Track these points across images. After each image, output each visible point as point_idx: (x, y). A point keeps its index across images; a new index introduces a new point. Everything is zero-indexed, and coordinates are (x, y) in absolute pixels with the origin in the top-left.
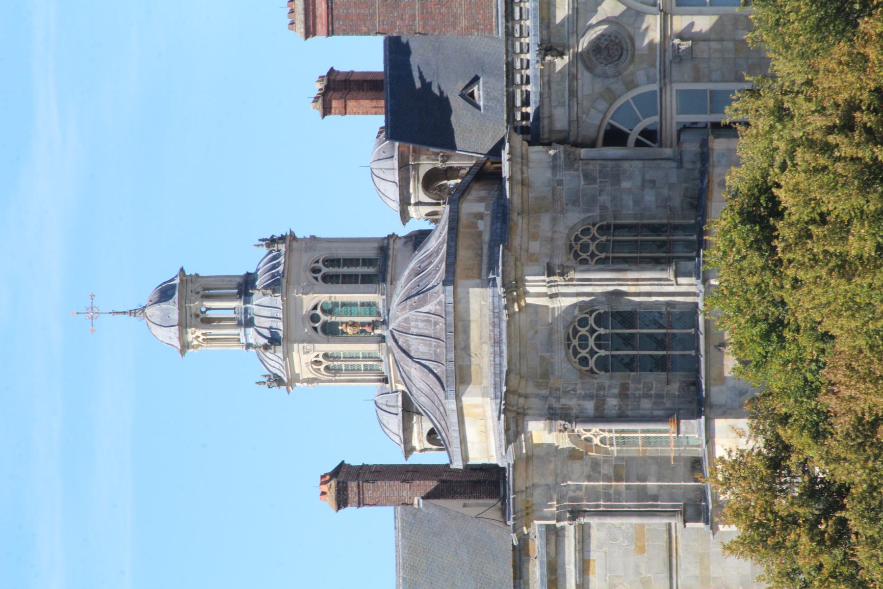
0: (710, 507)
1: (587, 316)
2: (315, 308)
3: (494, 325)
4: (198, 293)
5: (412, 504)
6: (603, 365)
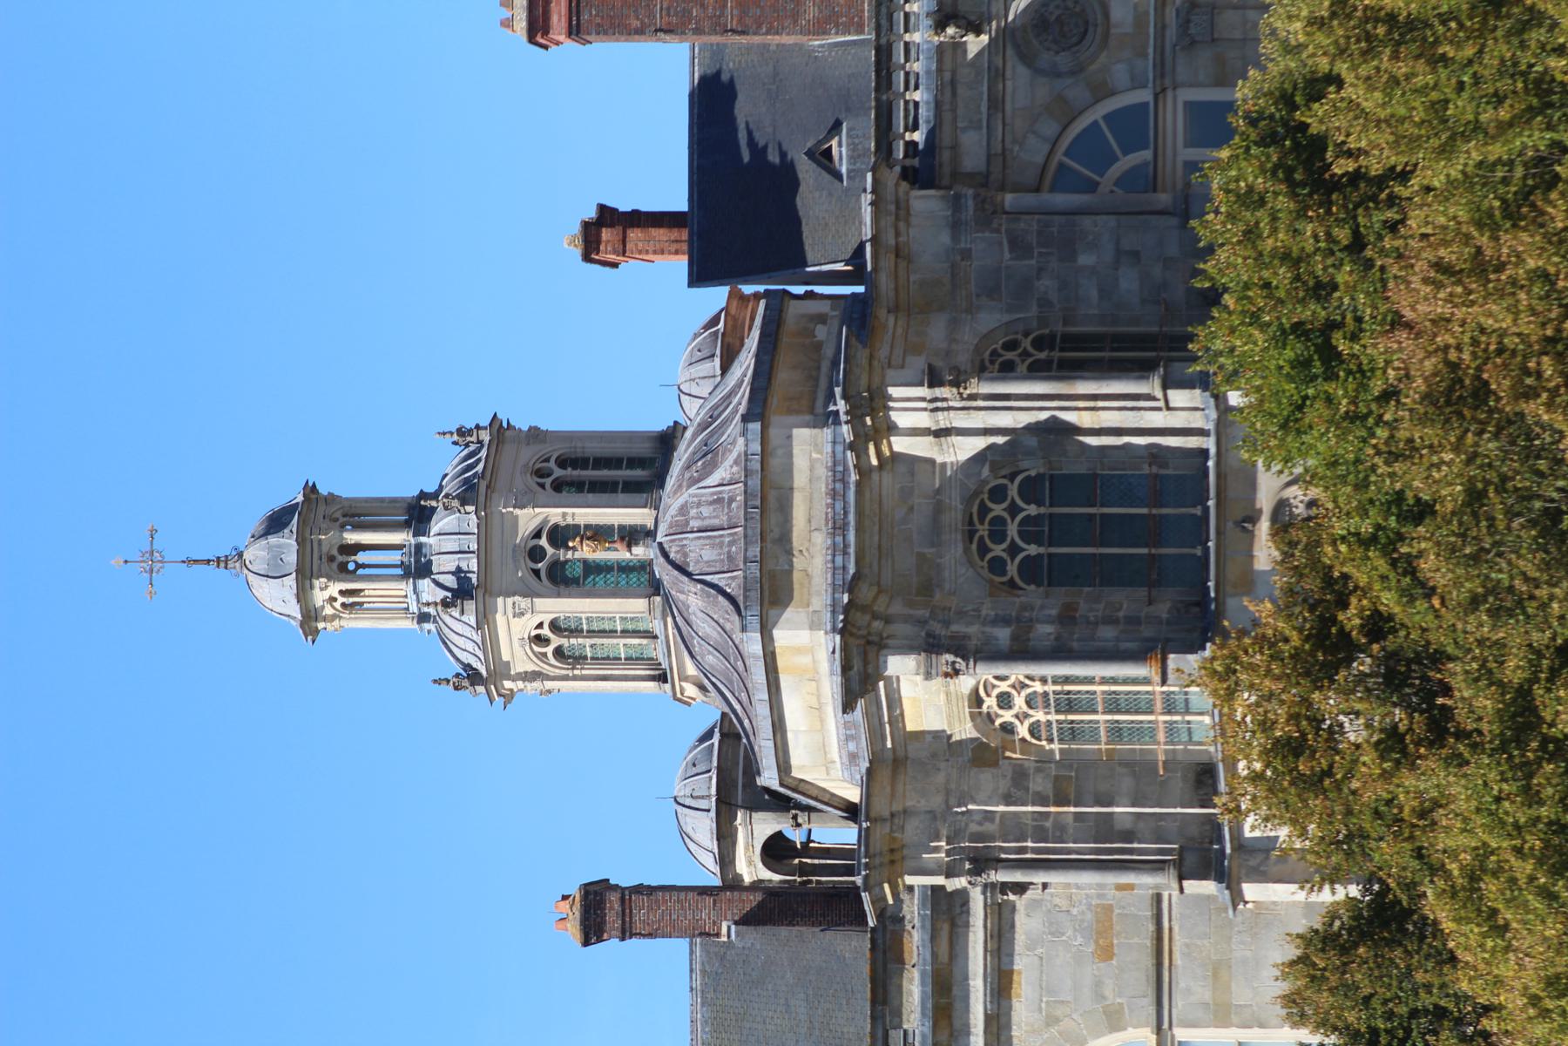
0: (1228, 851)
1: (1004, 481)
2: (537, 535)
3: (833, 494)
4: (337, 520)
5: (718, 935)
6: (1031, 570)
